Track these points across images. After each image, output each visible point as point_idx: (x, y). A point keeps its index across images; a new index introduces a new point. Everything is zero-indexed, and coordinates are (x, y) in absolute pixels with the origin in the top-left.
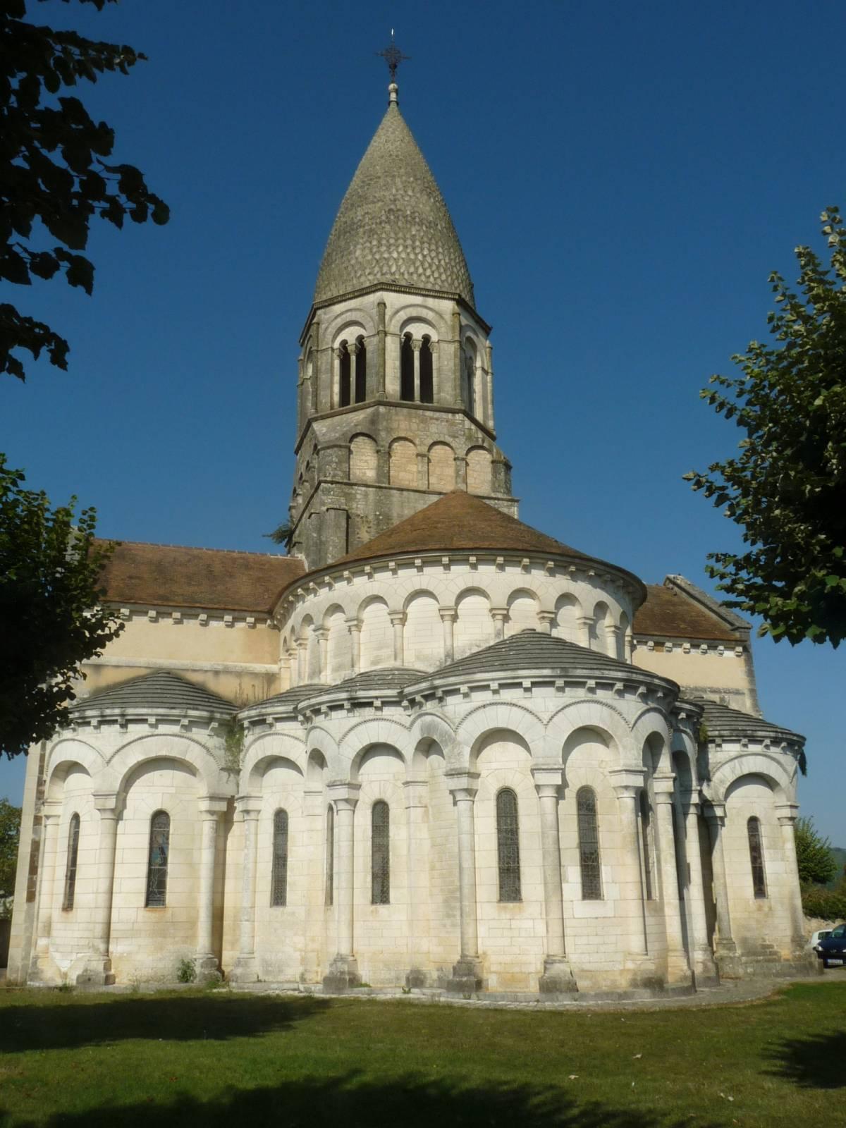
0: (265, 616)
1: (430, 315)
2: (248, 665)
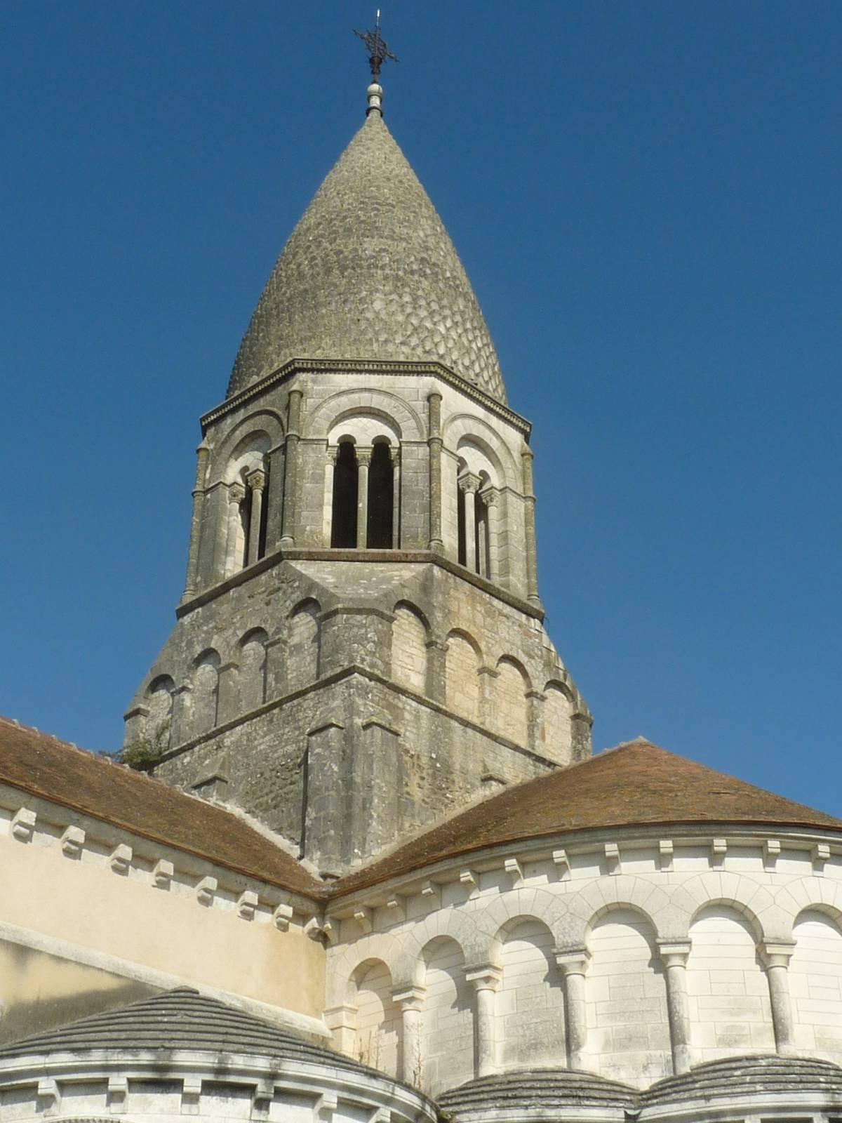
0: (311, 907)
1: (494, 443)
2: (285, 1011)
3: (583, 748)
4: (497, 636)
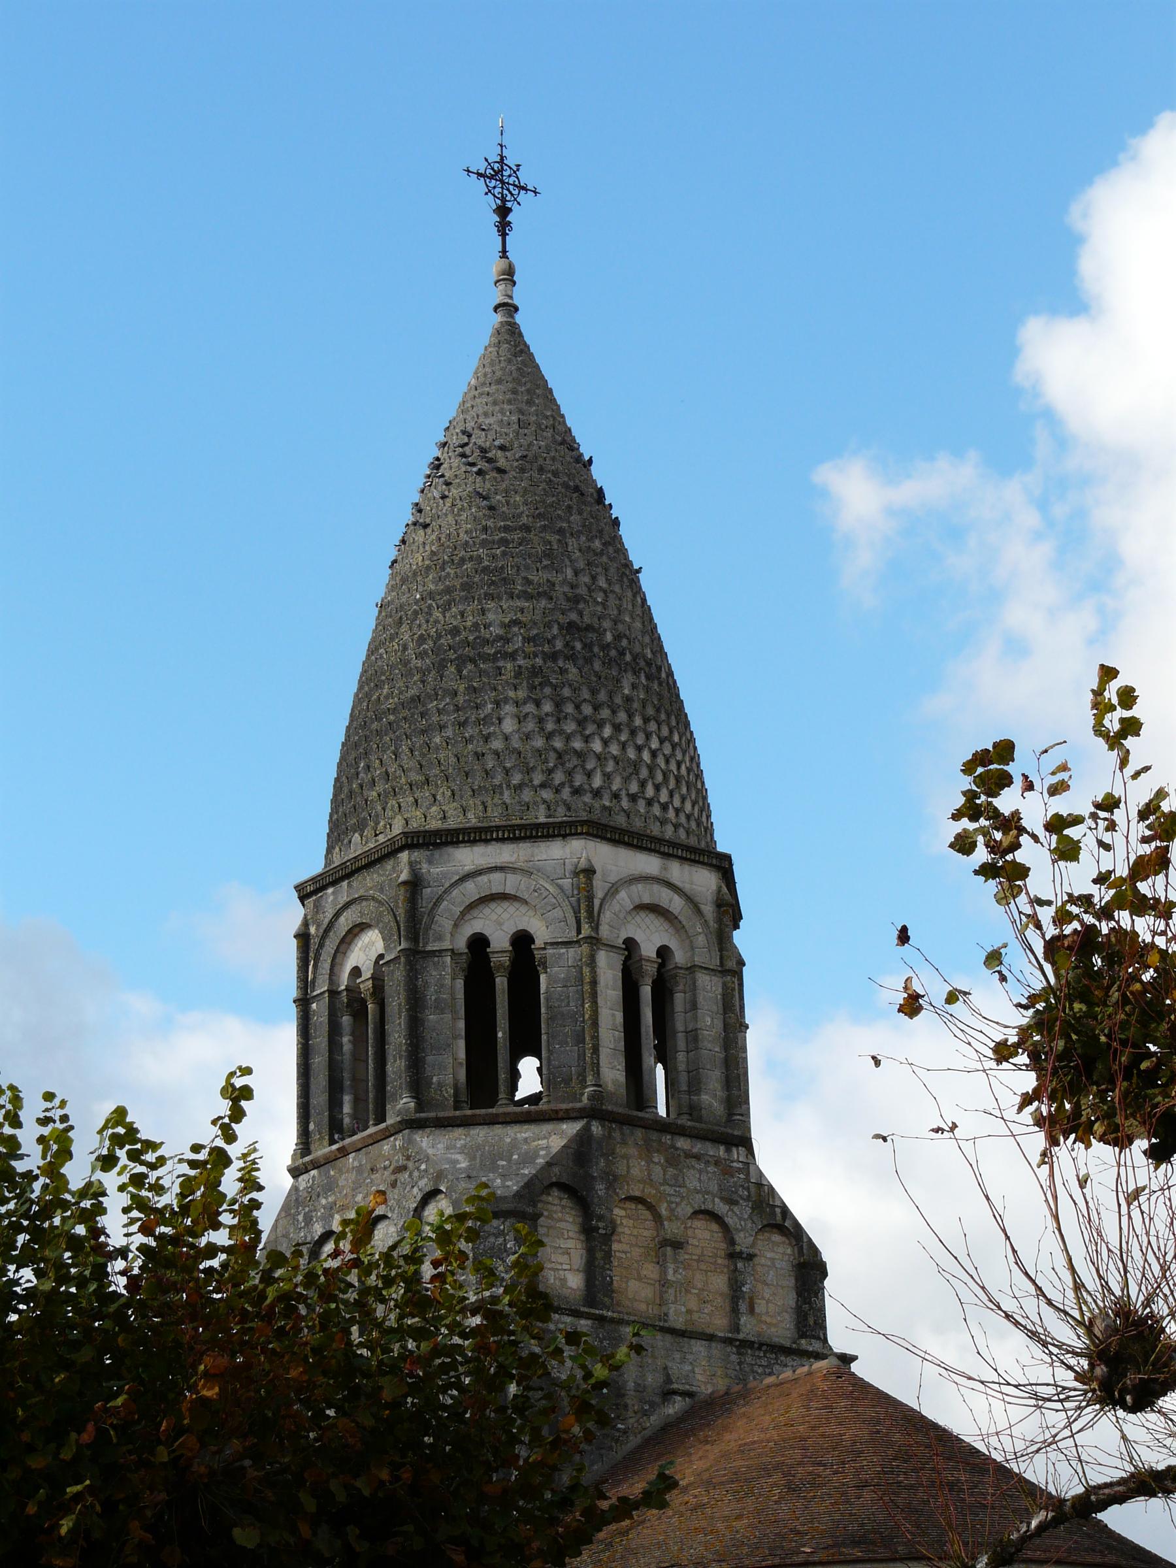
3: (811, 1308)
4: (682, 1190)
